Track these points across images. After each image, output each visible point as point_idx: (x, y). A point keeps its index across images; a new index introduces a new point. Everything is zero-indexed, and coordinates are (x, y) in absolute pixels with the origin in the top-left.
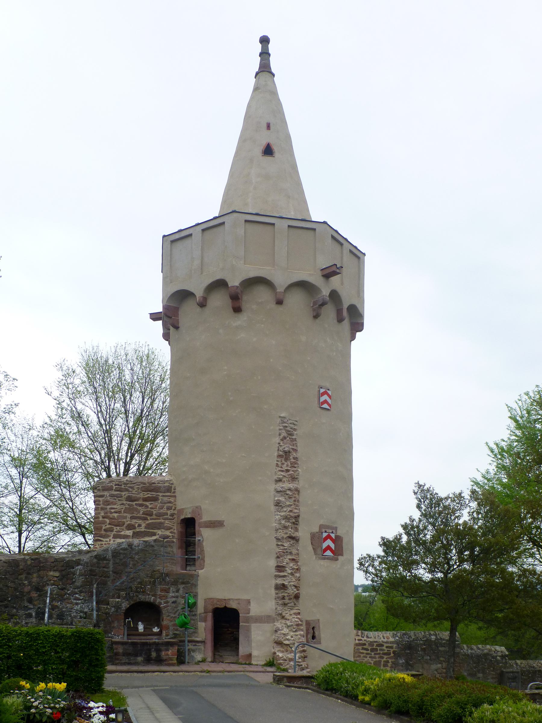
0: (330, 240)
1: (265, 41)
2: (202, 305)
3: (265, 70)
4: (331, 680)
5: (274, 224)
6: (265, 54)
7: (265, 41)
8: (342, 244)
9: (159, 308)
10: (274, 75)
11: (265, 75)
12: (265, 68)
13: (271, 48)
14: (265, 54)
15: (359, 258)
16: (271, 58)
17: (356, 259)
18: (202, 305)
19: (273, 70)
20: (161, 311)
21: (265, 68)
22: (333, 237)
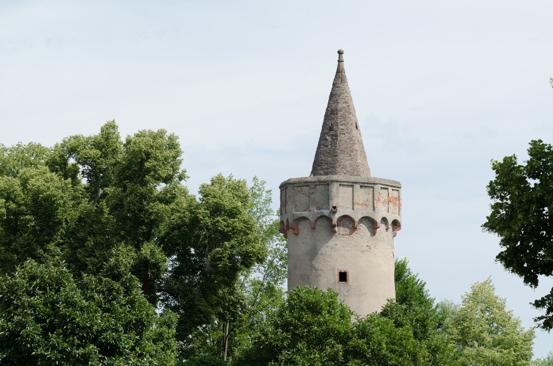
7: (340, 53)
13: (344, 56)
14: (340, 61)
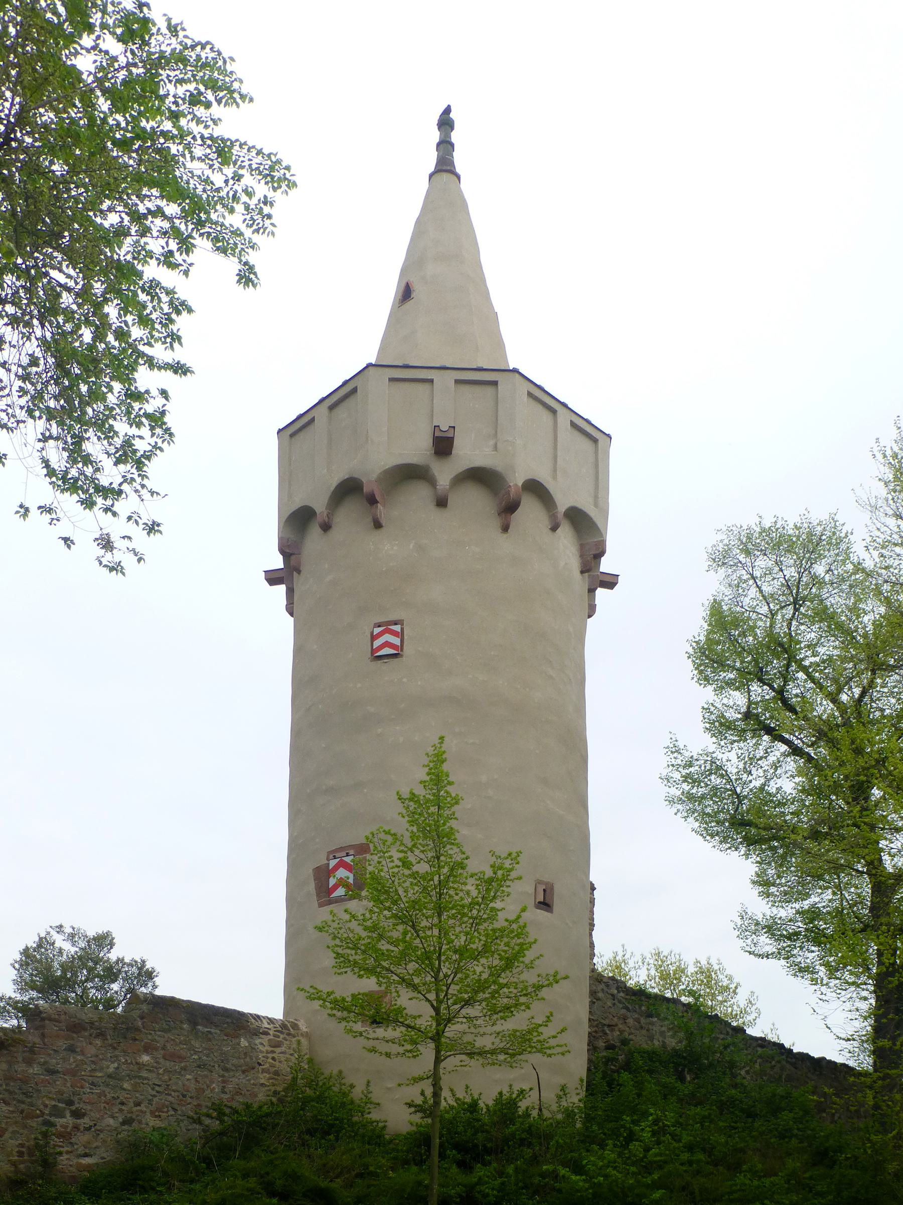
0: (525, 397)
1: (446, 122)
2: (326, 527)
3: (445, 168)
4: (573, 1111)
5: (432, 381)
6: (445, 146)
7: (446, 122)
8: (554, 412)
9: (277, 562)
10: (459, 177)
11: (445, 176)
12: (445, 165)
14: (445, 146)
15: (595, 441)
16: (454, 154)
17: (587, 444)
18: (326, 527)
19: (459, 169)
20: (282, 566)
21: (445, 165)
22: (530, 395)
